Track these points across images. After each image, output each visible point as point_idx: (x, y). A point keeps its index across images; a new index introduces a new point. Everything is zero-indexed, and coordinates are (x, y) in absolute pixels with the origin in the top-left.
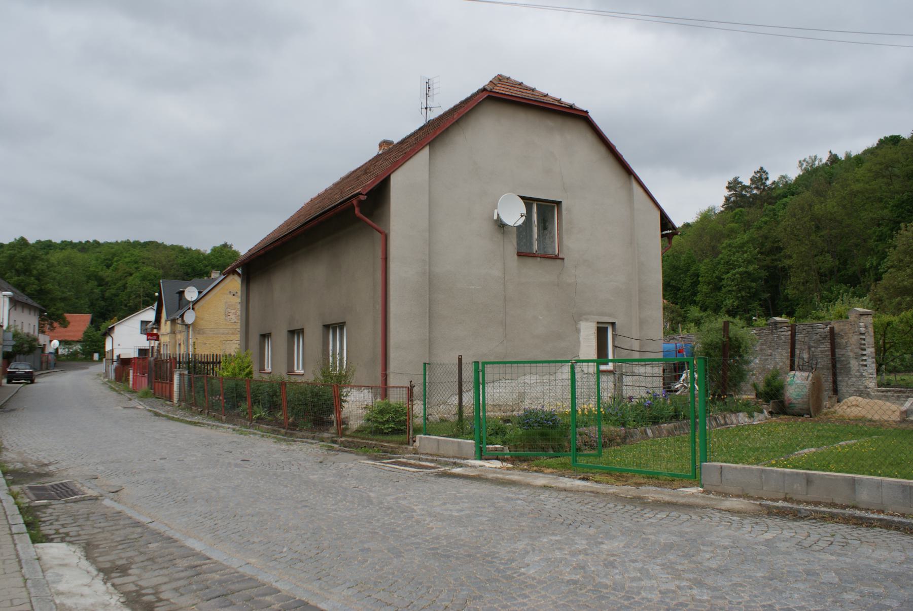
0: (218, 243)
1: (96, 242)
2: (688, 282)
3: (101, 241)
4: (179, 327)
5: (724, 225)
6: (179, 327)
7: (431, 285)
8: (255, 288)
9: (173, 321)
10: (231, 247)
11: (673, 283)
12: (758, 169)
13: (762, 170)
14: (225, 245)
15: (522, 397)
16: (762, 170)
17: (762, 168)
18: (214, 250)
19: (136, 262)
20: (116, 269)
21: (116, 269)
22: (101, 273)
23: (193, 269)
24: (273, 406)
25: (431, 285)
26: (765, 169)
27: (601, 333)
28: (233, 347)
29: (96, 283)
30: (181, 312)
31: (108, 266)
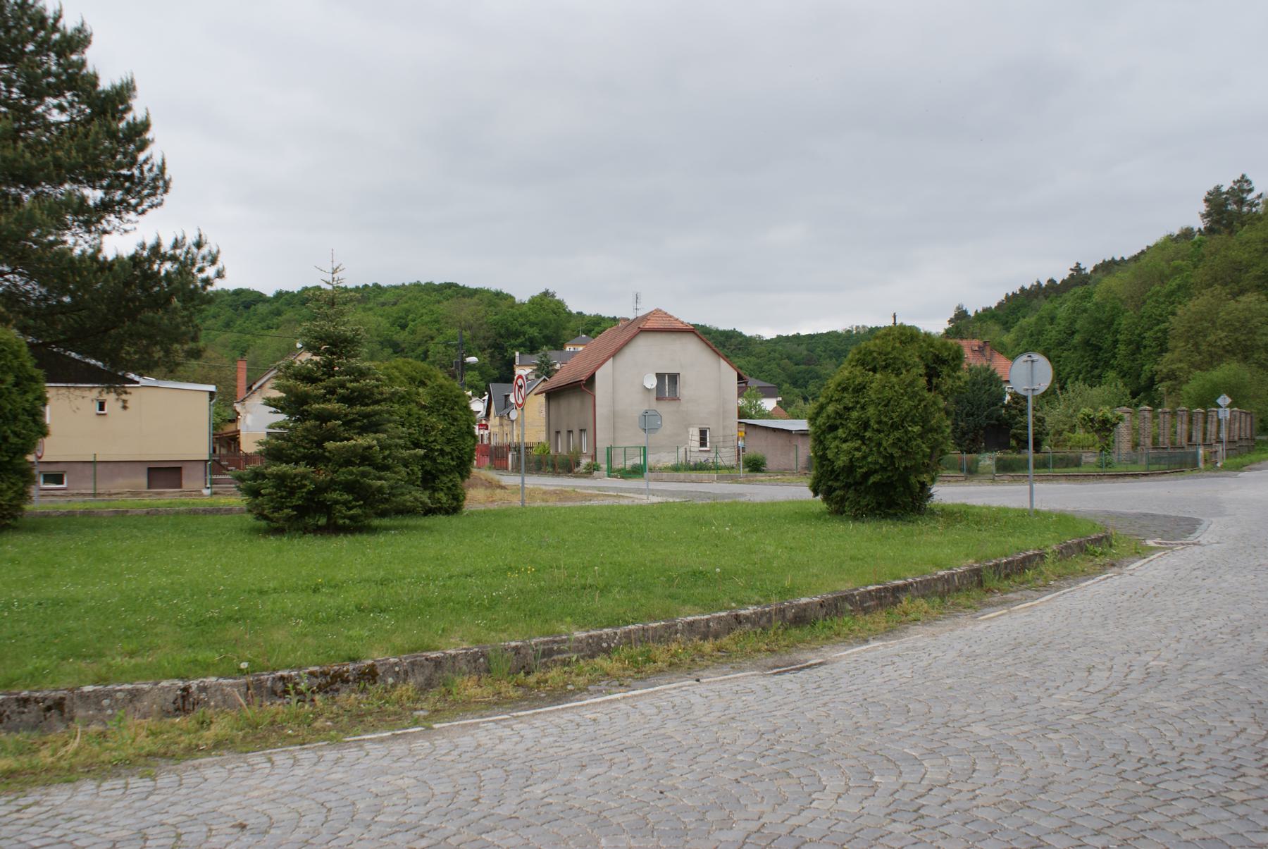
0: (537, 292)
1: (377, 286)
2: (1110, 338)
3: (384, 284)
4: (505, 422)
5: (1168, 262)
6: (505, 422)
7: (614, 415)
8: (553, 404)
9: (501, 417)
10: (553, 296)
11: (1093, 341)
12: (1238, 177)
13: (1243, 179)
14: (546, 294)
15: (658, 461)
16: (1243, 179)
17: (1243, 176)
18: (533, 301)
19: (436, 321)
20: (413, 332)
21: (413, 332)
22: (395, 337)
23: (507, 329)
24: (553, 466)
25: (614, 415)
26: (1249, 177)
27: (703, 433)
28: (542, 437)
29: (390, 351)
30: (507, 411)
31: (403, 327)
